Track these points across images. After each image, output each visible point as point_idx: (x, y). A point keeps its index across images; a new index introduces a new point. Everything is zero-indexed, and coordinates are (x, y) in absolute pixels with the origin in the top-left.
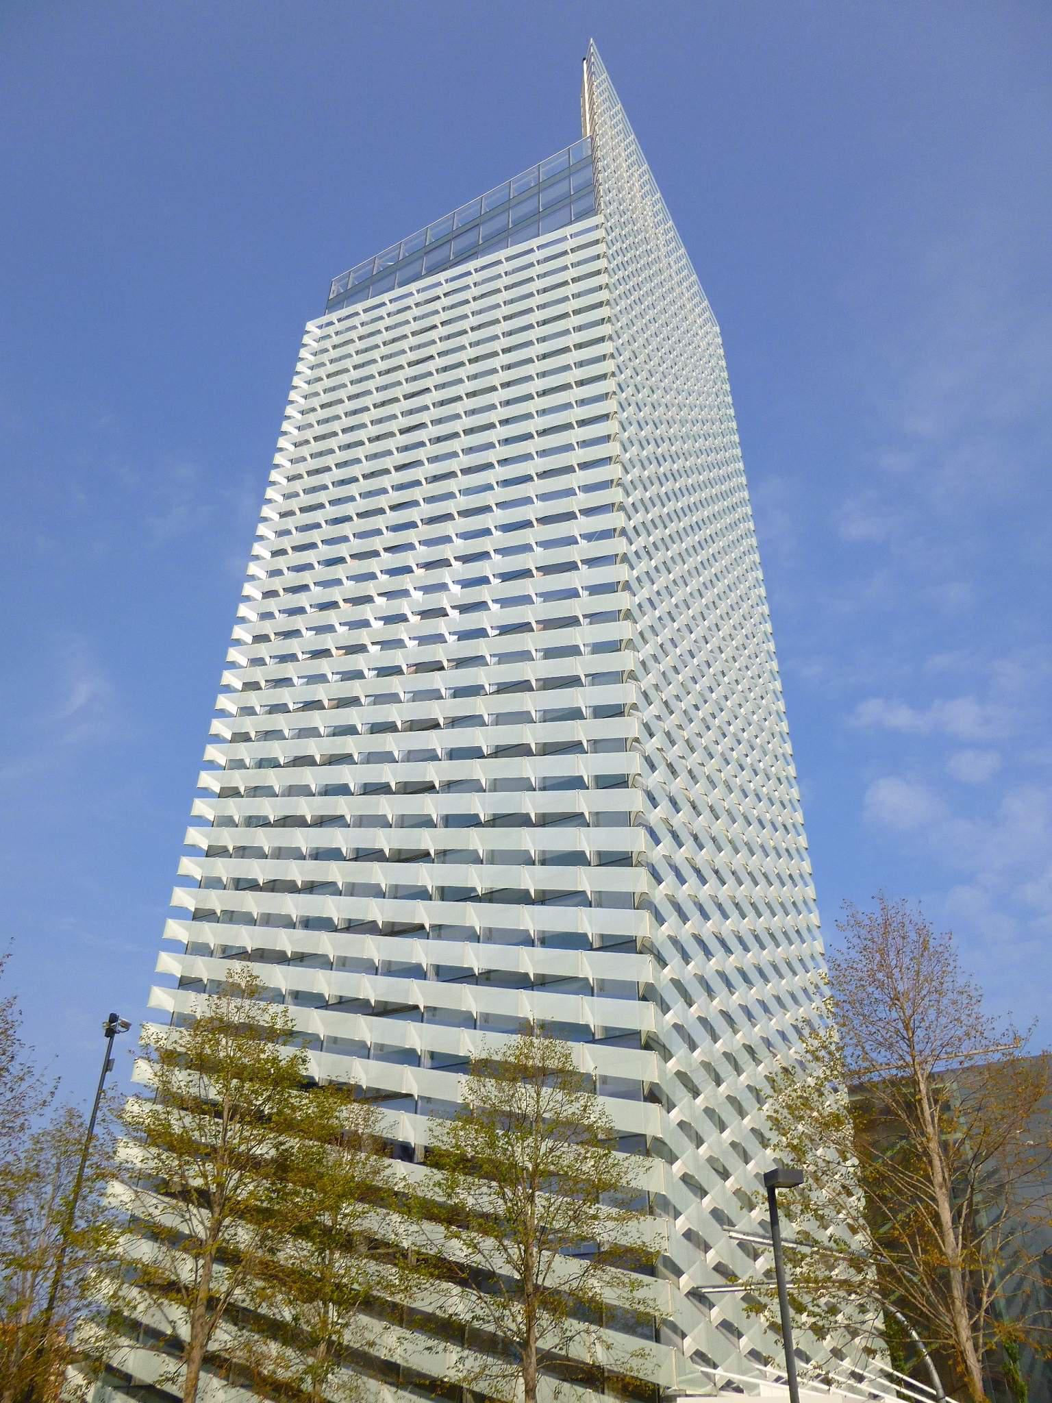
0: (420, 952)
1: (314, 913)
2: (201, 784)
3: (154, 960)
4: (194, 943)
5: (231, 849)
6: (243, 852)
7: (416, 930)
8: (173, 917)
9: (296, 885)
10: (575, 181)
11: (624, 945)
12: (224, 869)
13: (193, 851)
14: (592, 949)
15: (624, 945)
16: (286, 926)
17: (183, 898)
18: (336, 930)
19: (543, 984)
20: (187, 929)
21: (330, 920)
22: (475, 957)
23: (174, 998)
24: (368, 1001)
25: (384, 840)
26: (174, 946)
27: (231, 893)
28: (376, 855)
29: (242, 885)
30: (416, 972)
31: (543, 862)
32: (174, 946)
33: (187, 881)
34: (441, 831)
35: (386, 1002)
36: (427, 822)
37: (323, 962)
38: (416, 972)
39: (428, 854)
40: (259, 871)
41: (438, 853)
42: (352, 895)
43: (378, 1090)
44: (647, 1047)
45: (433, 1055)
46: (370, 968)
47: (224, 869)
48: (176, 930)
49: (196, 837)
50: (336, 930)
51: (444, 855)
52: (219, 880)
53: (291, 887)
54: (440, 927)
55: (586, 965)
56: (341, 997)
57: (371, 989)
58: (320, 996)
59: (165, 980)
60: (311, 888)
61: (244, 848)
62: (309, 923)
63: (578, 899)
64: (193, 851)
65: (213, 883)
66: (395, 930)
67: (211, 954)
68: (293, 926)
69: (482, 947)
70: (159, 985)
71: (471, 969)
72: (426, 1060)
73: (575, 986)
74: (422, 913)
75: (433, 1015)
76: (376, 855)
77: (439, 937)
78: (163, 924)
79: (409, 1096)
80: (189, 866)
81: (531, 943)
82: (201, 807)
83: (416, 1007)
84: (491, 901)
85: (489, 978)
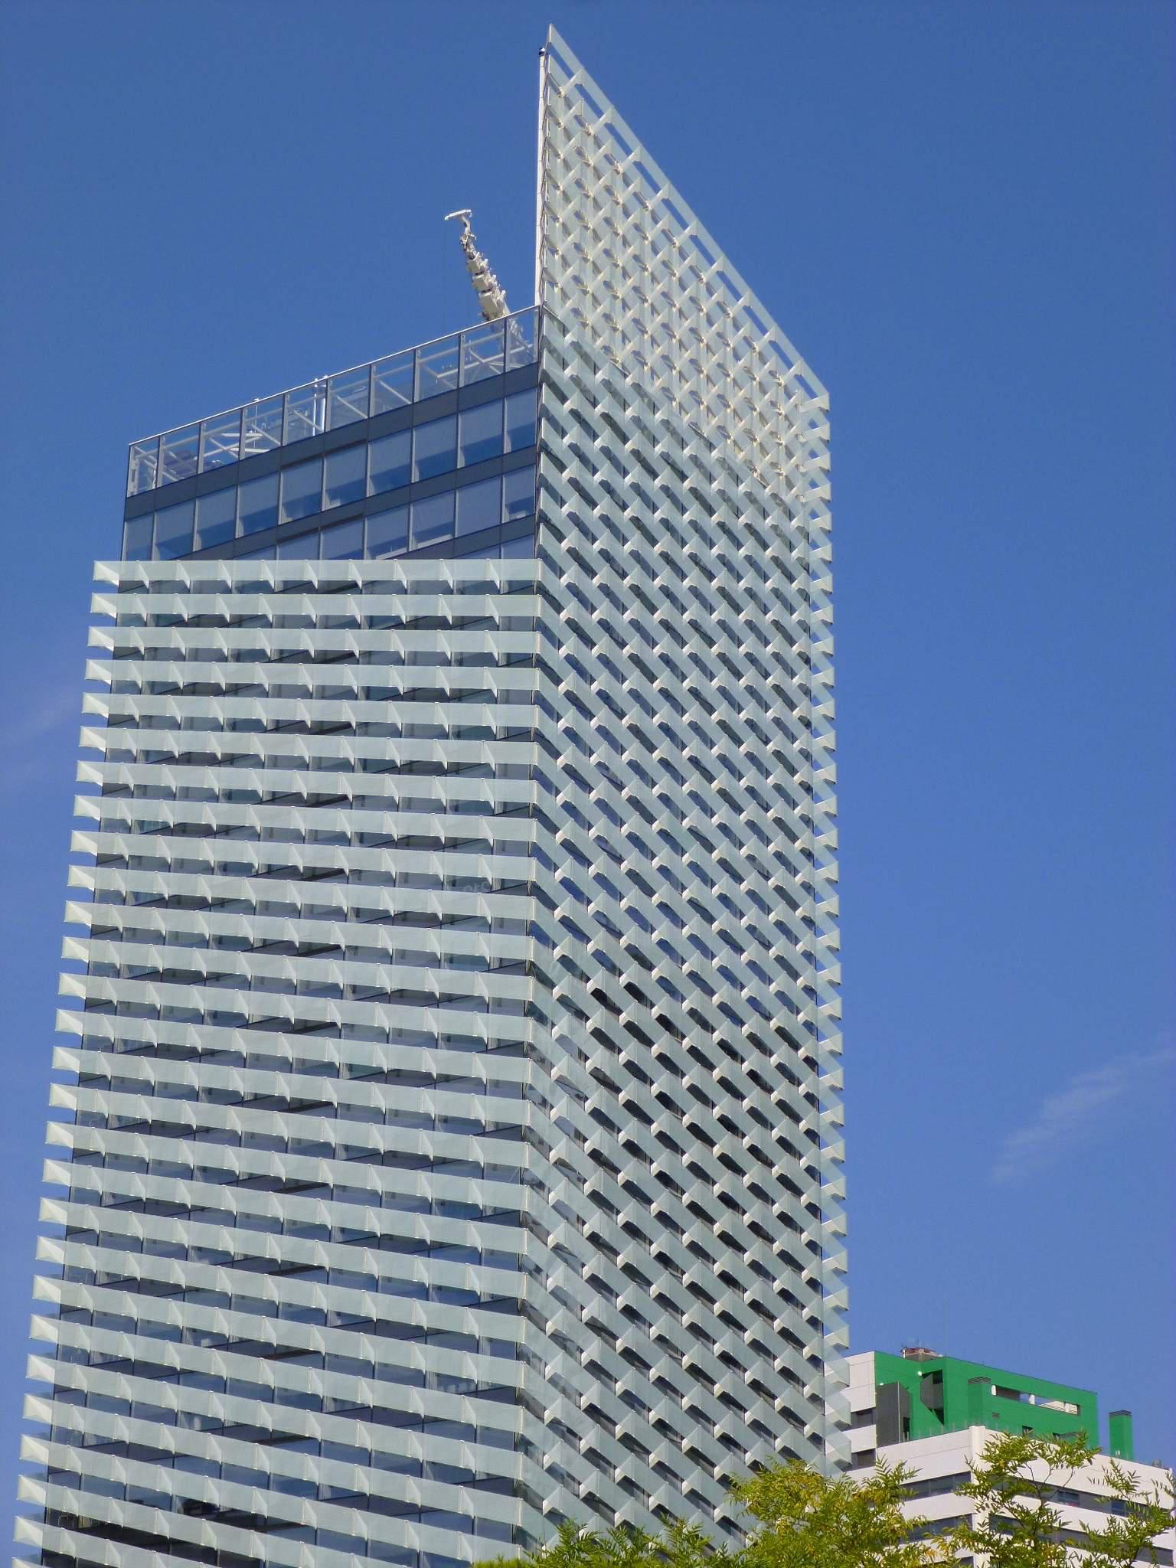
1: (241, 715)
2: (92, 642)
3: (83, 668)
4: (107, 820)
5: (147, 583)
6: (154, 654)
8: (90, 691)
10: (470, 429)
11: (509, 1217)
12: (136, 672)
14: (489, 971)
15: (509, 1217)
16: (214, 729)
17: (100, 637)
18: (261, 802)
19: (452, 923)
21: (259, 722)
22: (386, 977)
23: (83, 1021)
25: (309, 641)
26: (87, 824)
27: (152, 630)
28: (300, 656)
29: (158, 689)
30: (341, 839)
31: (462, 592)
32: (87, 824)
34: (363, 703)
35: (322, 722)
36: (351, 623)
38: (341, 839)
40: (178, 673)
41: (362, 654)
42: (283, 627)
43: (297, 1181)
44: (519, 1312)
45: (347, 1148)
48: (69, 1021)
49: (100, 637)
50: (273, 592)
51: (369, 657)
52: (134, 684)
53: (215, 690)
54: (363, 797)
55: (478, 1150)
56: (274, 793)
57: (290, 1007)
58: (245, 940)
60: (235, 690)
61: (160, 582)
62: (231, 796)
63: (483, 771)
66: (323, 729)
68: (221, 729)
69: (401, 815)
71: (393, 761)
74: (337, 933)
75: (349, 1031)
76: (300, 656)
77: (366, 734)
78: (87, 633)
79: (321, 1268)
81: (444, 810)
82: (102, 603)
83: (330, 1104)
84: (416, 628)
85: (396, 1077)
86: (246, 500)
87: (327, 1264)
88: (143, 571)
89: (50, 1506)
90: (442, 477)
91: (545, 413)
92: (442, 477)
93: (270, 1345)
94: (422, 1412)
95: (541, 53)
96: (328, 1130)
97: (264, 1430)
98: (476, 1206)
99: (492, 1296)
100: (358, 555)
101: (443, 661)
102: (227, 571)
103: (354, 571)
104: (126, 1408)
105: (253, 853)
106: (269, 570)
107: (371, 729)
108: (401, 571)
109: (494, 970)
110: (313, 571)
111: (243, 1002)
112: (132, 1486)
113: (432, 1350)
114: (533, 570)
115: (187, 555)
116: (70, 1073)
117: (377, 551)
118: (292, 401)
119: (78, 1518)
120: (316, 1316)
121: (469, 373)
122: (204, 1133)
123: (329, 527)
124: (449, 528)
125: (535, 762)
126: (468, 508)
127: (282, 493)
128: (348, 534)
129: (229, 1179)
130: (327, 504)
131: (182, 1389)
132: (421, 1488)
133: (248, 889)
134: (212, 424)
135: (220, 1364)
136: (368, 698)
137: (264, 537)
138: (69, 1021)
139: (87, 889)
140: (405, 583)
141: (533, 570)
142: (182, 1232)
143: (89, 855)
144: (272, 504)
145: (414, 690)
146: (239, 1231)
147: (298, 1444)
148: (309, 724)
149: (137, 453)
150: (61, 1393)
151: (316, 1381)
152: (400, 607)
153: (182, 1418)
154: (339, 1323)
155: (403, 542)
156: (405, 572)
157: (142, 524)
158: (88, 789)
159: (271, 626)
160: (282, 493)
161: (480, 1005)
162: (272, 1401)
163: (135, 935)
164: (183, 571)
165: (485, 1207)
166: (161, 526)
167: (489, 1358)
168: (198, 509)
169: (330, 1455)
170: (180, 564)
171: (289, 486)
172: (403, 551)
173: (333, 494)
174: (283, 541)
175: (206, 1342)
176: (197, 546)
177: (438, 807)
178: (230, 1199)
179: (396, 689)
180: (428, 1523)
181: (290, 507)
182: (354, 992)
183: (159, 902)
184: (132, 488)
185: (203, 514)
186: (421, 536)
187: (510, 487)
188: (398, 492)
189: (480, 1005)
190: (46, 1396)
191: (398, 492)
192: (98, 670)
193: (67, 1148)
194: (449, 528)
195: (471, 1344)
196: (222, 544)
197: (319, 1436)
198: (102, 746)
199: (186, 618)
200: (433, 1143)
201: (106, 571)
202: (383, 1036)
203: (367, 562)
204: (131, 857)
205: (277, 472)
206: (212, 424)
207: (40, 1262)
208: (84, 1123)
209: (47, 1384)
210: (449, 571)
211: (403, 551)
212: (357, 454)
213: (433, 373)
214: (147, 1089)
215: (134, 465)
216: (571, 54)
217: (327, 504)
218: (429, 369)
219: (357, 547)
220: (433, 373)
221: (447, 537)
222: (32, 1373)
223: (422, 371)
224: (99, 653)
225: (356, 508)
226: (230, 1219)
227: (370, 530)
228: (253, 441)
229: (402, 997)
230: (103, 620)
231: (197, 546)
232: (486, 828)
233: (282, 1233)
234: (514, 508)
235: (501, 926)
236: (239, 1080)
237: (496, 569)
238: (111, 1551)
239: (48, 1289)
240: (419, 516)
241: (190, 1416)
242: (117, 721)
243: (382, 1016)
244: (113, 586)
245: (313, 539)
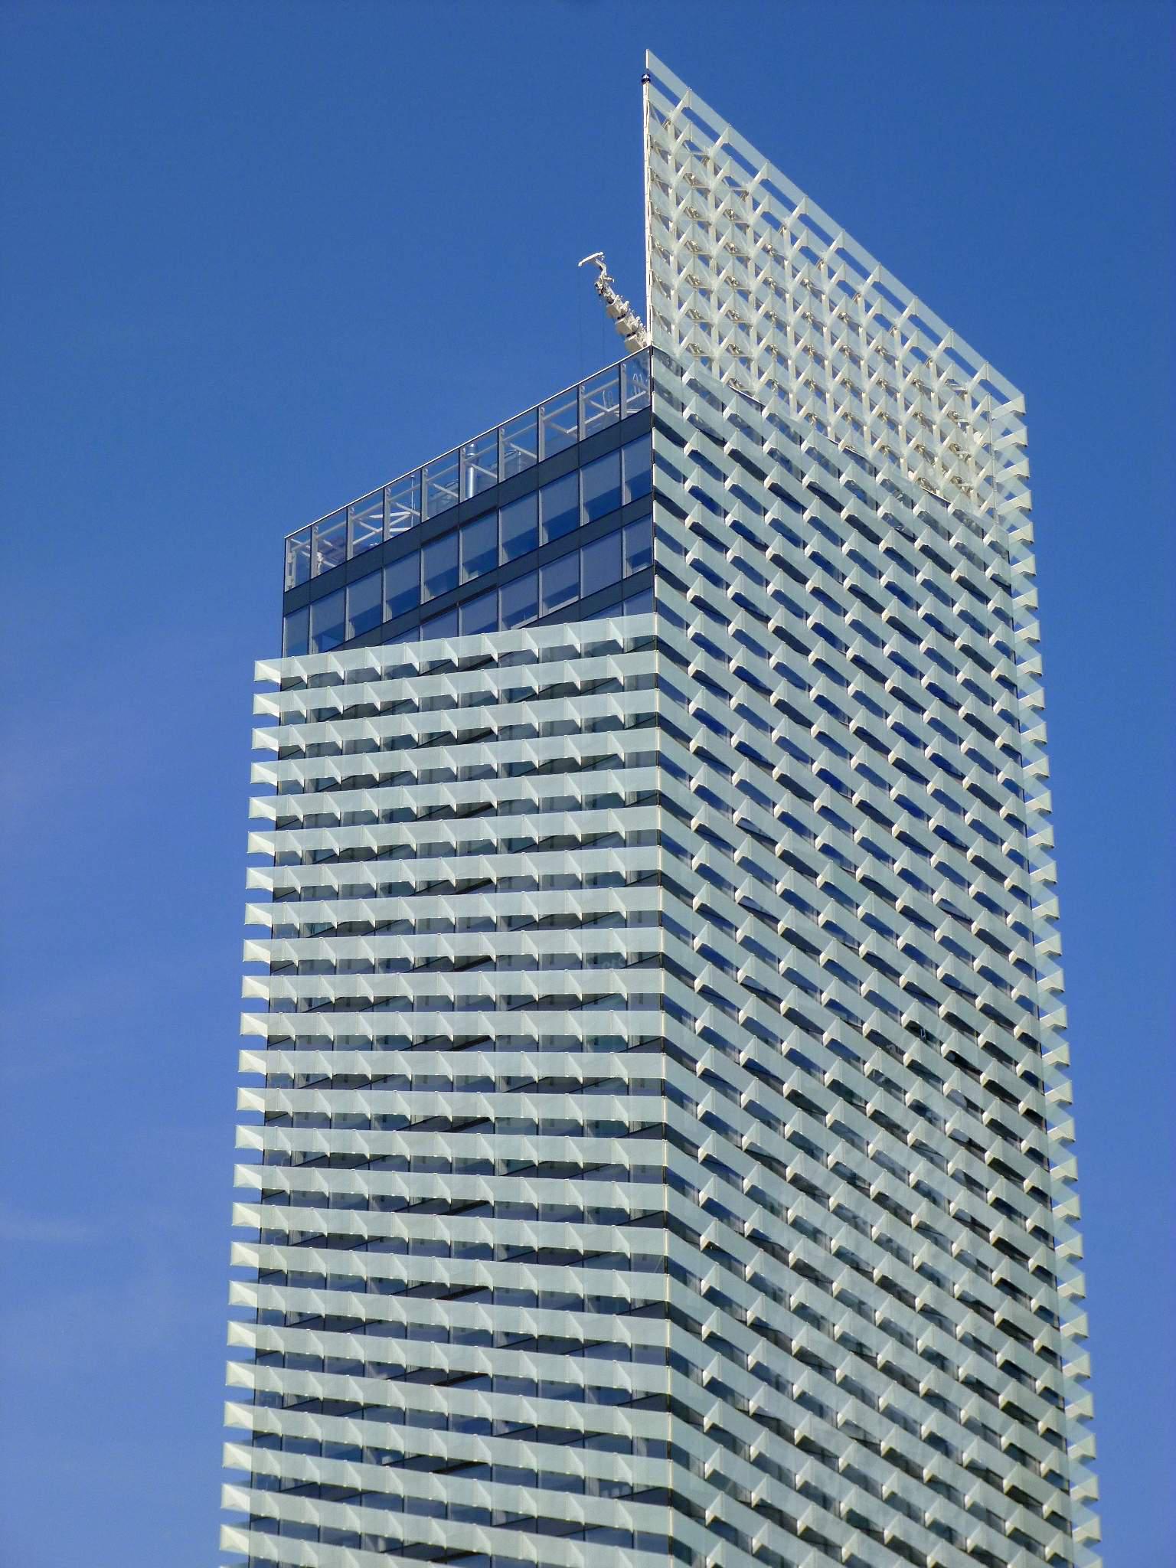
0: (485, 1064)
2: (257, 710)
5: (305, 679)
7: (484, 809)
9: (375, 708)
10: (590, 485)
13: (266, 686)
14: (627, 967)
20: (268, 984)
22: (531, 1066)
24: (446, 1118)
26: (259, 932)
30: (484, 1167)
32: (259, 932)
33: (263, 789)
36: (488, 773)
37: (404, 1004)
39: (491, 659)
40: (334, 768)
46: (447, 1085)
47: (300, 702)
48: (255, 987)
57: (447, 1025)
59: (246, 1195)
64: (264, 755)
65: (291, 788)
67: (298, 934)
70: (242, 1123)
72: (502, 1085)
73: (612, 1086)
74: (485, 1024)
80: (263, 773)
86: (390, 583)
87: (489, 1459)
88: (300, 667)
89: (252, 1555)
90: (568, 535)
91: (658, 459)
92: (568, 535)
93: (441, 1459)
94: (582, 1520)
95: (644, 81)
96: (484, 1230)
97: (439, 1548)
98: (623, 1300)
99: (646, 1301)
100: (493, 628)
101: (574, 883)
102: (375, 657)
103: (488, 645)
104: (317, 1364)
105: (407, 947)
106: (413, 652)
107: (515, 732)
108: (530, 639)
109: (633, 966)
110: (451, 649)
111: (403, 1104)
112: (326, 1529)
113: (590, 1454)
114: (652, 624)
115: (342, 645)
116: (253, 1190)
117: (512, 621)
118: (431, 473)
119: (282, 1398)
120: (482, 1338)
121: (588, 426)
122: (380, 1162)
123: (465, 602)
124: (574, 590)
125: (662, 1033)
126: (589, 568)
127: (420, 572)
128: (482, 608)
129: (400, 1289)
130: (464, 577)
131: (366, 1423)
132: (584, 1506)
133: (405, 985)
134: (359, 507)
135: (396, 1481)
136: (510, 701)
137: (412, 619)
138: (249, 1137)
139: (264, 926)
140: (536, 726)
141: (652, 624)
142: (356, 1347)
143: (265, 891)
144: (413, 585)
145: (552, 687)
146: (410, 1343)
147: (471, 1470)
148: (454, 883)
149: (293, 544)
150: (261, 1439)
151: (483, 1494)
152: (531, 677)
153: (366, 1540)
154: (507, 1430)
155: (533, 609)
156: (536, 640)
157: (301, 616)
158: (261, 824)
159: (417, 710)
160: (420, 572)
161: (622, 1262)
162: (447, 1429)
163: (316, 821)
164: (336, 662)
165: (633, 1300)
166: (315, 618)
167: (645, 1459)
168: (348, 598)
169: (503, 1301)
170: (331, 656)
171: (426, 565)
172: (534, 618)
173: (471, 567)
174: (426, 621)
175: (386, 1459)
176: (350, 633)
177: (573, 883)
178: (400, 1226)
179: (530, 763)
180: (592, 1540)
181: (431, 584)
182: (509, 1003)
183: (326, 1006)
184: (290, 582)
185: (353, 601)
186: (551, 601)
187: (627, 542)
188: (529, 556)
189: (621, 1174)
190: (245, 1443)
191: (529, 556)
192: (260, 843)
193: (253, 1268)
194: (574, 590)
195: (624, 1445)
196: (373, 631)
197: (490, 1461)
198: (273, 779)
199: (337, 852)
200: (582, 1150)
201: (268, 670)
202: (533, 1128)
203: (502, 634)
204: (299, 1037)
205: (417, 551)
206: (359, 507)
207: (231, 1347)
208: (269, 1242)
209: (246, 1431)
210: (574, 634)
211: (534, 618)
212: (489, 600)
213: (559, 428)
214: (321, 1201)
215: (290, 558)
216: (669, 72)
217: (464, 577)
218: (554, 425)
219: (492, 620)
220: (559, 428)
221: (575, 599)
222: (232, 1340)
223: (547, 428)
224: (264, 755)
225: (492, 579)
226: (401, 1331)
227: (503, 601)
228: (399, 520)
229: (552, 1003)
230: (266, 720)
231: (350, 633)
232: (619, 1066)
233: (448, 1342)
234: (635, 561)
235: (641, 1002)
236: (402, 1185)
237: (617, 628)
238: (309, 1551)
239: (240, 1416)
240: (544, 582)
241: (374, 1538)
242: (284, 824)
243: (530, 1024)
244: (274, 684)
245: (452, 617)
